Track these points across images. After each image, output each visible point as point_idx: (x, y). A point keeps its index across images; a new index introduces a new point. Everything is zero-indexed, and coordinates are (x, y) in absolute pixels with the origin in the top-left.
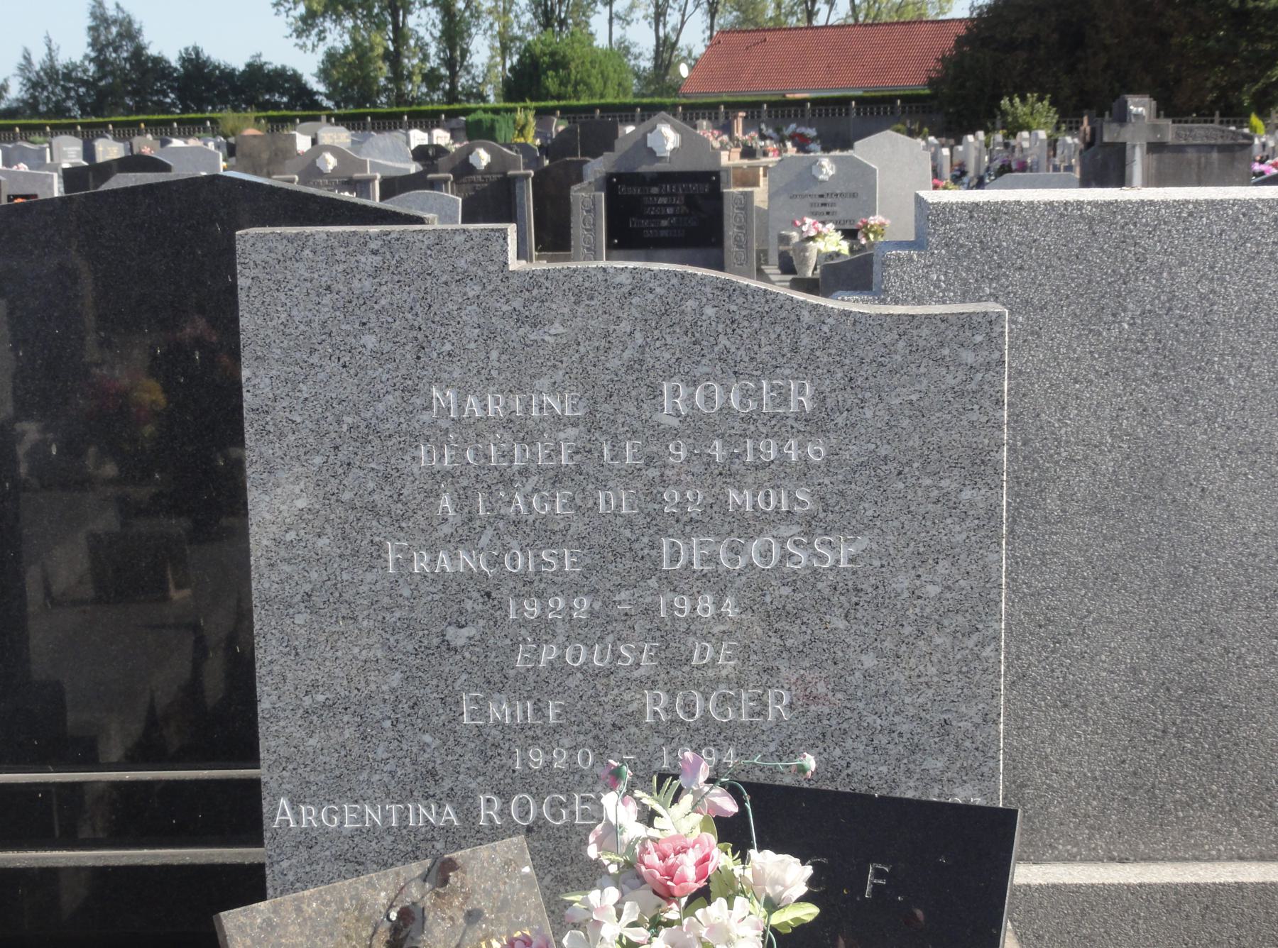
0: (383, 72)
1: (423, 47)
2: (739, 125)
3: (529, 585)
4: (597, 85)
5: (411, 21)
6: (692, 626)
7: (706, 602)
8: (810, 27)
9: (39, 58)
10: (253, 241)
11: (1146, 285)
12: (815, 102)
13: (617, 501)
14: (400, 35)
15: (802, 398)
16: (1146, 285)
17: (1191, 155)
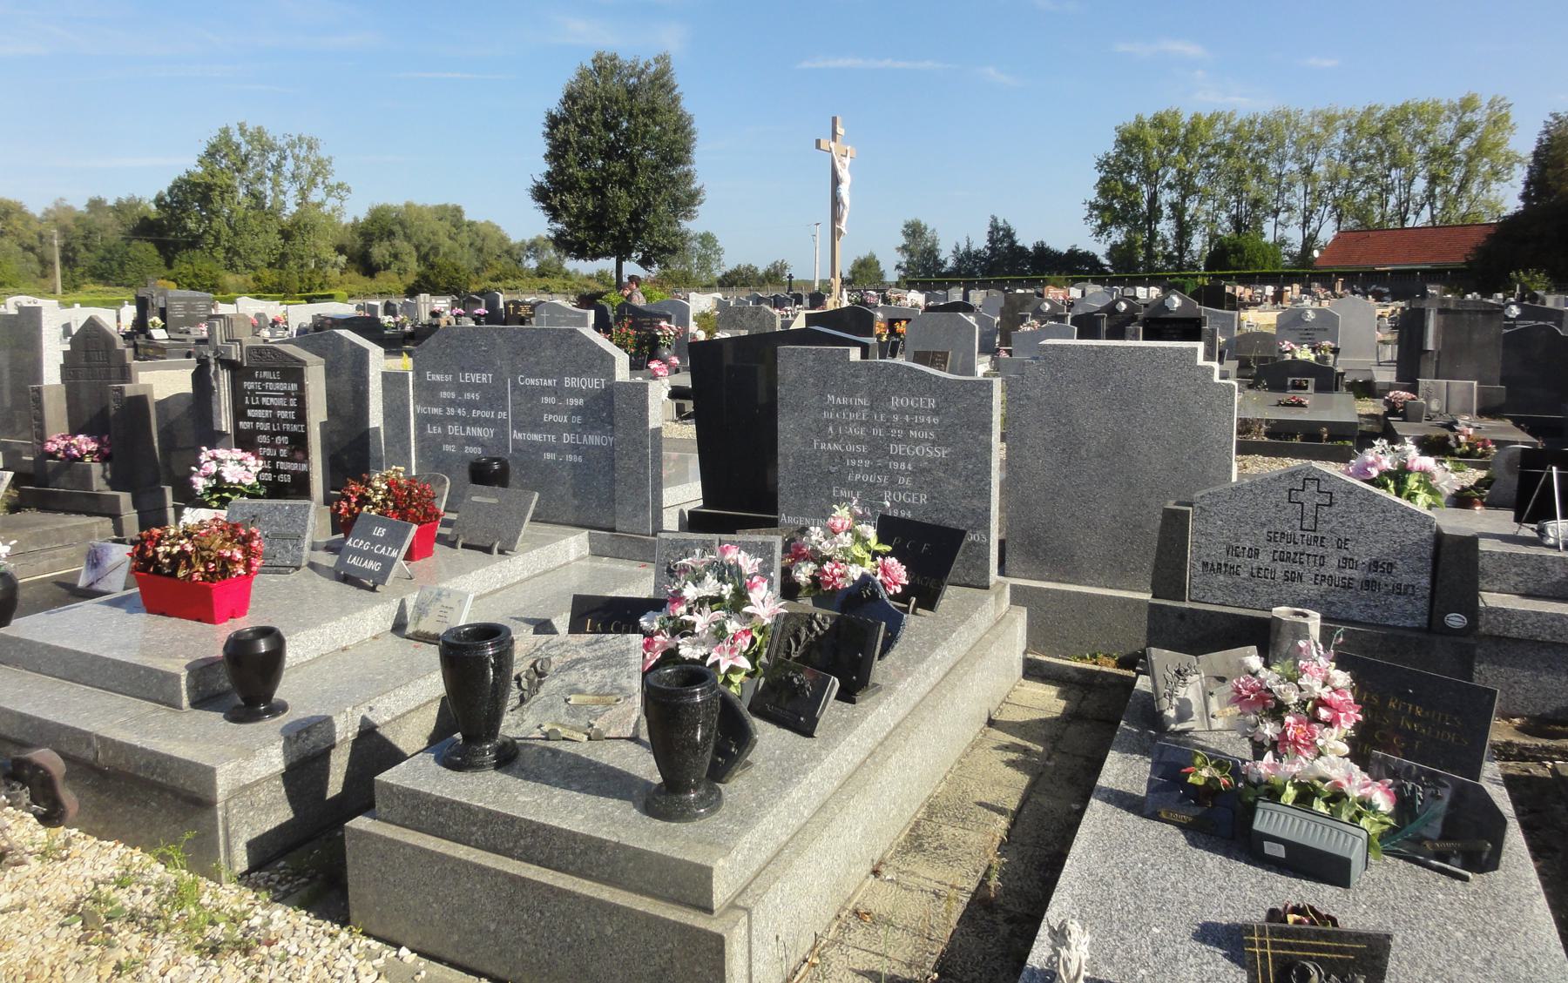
0: (1141, 255)
1: (1164, 241)
2: (1339, 285)
3: (855, 456)
4: (1260, 261)
5: (1159, 227)
6: (899, 472)
7: (903, 465)
8: (1403, 228)
9: (963, 247)
10: (783, 349)
11: (1116, 376)
12: (1393, 272)
13: (878, 432)
14: (1153, 234)
15: (932, 404)
16: (1116, 376)
17: (1466, 316)
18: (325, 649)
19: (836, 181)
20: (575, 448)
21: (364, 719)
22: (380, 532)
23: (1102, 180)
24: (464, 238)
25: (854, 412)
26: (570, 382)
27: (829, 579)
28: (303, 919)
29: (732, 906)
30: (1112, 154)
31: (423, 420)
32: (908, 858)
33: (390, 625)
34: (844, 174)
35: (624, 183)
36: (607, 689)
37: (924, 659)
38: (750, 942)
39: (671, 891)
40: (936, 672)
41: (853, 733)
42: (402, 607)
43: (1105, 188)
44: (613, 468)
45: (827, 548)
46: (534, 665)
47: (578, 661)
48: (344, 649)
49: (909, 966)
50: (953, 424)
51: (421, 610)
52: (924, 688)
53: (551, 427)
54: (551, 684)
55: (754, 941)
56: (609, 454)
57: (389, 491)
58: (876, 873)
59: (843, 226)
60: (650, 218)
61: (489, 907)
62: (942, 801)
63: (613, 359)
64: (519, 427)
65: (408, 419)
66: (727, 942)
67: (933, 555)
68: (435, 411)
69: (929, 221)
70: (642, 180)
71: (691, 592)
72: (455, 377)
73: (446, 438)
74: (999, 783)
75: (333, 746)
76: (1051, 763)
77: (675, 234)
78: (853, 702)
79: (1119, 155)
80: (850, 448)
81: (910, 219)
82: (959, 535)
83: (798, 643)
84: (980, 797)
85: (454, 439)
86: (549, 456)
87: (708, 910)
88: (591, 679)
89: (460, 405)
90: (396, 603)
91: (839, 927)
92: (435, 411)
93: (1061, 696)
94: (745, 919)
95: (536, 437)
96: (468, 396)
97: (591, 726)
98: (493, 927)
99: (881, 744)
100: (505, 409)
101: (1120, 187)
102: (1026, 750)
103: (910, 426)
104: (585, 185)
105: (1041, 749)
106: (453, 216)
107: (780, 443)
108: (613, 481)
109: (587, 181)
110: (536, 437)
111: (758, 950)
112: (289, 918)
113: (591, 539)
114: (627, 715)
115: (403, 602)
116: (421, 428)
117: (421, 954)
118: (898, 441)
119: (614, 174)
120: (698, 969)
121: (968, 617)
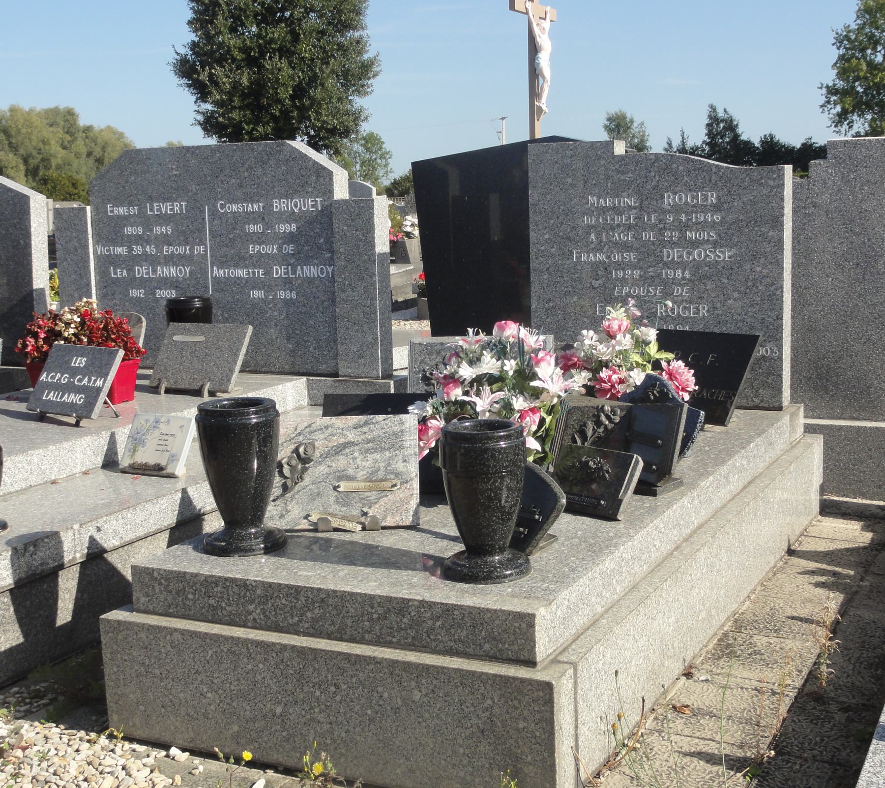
3: (620, 266)
6: (674, 282)
7: (679, 273)
13: (649, 236)
15: (713, 199)
18: (34, 480)
19: (534, 49)
20: (287, 283)
21: (92, 540)
22: (80, 362)
23: (842, 58)
24: (80, 146)
25: (620, 214)
26: (280, 205)
27: (607, 386)
28: (54, 731)
29: (555, 661)
30: (854, 26)
31: (104, 263)
32: (721, 662)
33: (100, 460)
34: (544, 40)
35: (284, 52)
36: (381, 474)
37: (723, 462)
38: (576, 699)
39: (487, 647)
40: (736, 483)
41: (649, 530)
42: (112, 442)
43: (845, 67)
44: (333, 302)
45: (603, 351)
46: (296, 451)
47: (345, 446)
48: (54, 482)
49: (741, 747)
50: (737, 221)
51: (136, 441)
52: (724, 494)
53: (260, 260)
54: (316, 471)
55: (580, 700)
56: (330, 292)
57: (82, 324)
58: (688, 675)
59: (543, 103)
60: (317, 93)
61: (275, 688)
62: (749, 616)
63: (330, 174)
64: (222, 263)
65: (88, 262)
66: (556, 690)
67: (726, 367)
68: (120, 250)
69: (636, 113)
70: (305, 49)
71: (467, 372)
72: (142, 209)
73: (133, 282)
74: (811, 601)
75: (61, 567)
76: (866, 583)
77: (347, 113)
78: (654, 494)
79: (861, 28)
80: (617, 257)
81: (613, 110)
82: (750, 341)
83: (584, 438)
84: (790, 612)
85: (142, 283)
86: (257, 294)
87: (531, 663)
88: (362, 464)
89: (148, 242)
90: (105, 436)
91: (656, 719)
92: (120, 250)
93: (865, 528)
94: (571, 672)
95: (241, 273)
96: (158, 230)
97: (365, 514)
98: (279, 710)
99: (686, 540)
100: (202, 242)
101: (864, 67)
102: (835, 574)
103: (687, 226)
104: (239, 56)
105: (852, 573)
106: (65, 120)
107: (532, 256)
108: (334, 317)
109: (240, 50)
110: (241, 273)
111: (583, 716)
112: (38, 730)
113: (309, 387)
114: (405, 501)
115: (113, 435)
116: (102, 273)
117: (194, 752)
118: (673, 244)
119: (272, 41)
120: (521, 725)
121: (764, 431)
